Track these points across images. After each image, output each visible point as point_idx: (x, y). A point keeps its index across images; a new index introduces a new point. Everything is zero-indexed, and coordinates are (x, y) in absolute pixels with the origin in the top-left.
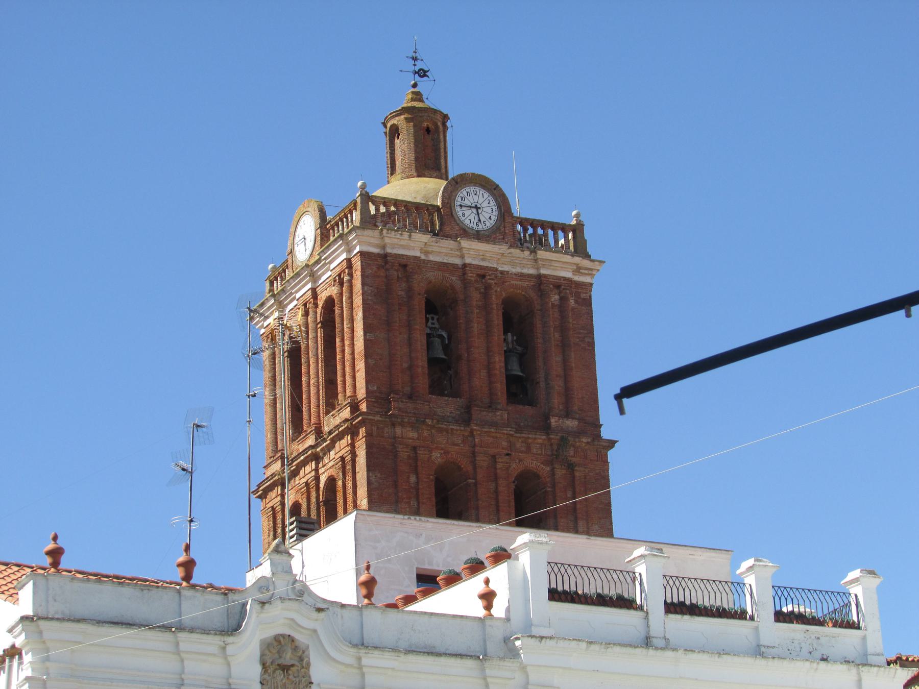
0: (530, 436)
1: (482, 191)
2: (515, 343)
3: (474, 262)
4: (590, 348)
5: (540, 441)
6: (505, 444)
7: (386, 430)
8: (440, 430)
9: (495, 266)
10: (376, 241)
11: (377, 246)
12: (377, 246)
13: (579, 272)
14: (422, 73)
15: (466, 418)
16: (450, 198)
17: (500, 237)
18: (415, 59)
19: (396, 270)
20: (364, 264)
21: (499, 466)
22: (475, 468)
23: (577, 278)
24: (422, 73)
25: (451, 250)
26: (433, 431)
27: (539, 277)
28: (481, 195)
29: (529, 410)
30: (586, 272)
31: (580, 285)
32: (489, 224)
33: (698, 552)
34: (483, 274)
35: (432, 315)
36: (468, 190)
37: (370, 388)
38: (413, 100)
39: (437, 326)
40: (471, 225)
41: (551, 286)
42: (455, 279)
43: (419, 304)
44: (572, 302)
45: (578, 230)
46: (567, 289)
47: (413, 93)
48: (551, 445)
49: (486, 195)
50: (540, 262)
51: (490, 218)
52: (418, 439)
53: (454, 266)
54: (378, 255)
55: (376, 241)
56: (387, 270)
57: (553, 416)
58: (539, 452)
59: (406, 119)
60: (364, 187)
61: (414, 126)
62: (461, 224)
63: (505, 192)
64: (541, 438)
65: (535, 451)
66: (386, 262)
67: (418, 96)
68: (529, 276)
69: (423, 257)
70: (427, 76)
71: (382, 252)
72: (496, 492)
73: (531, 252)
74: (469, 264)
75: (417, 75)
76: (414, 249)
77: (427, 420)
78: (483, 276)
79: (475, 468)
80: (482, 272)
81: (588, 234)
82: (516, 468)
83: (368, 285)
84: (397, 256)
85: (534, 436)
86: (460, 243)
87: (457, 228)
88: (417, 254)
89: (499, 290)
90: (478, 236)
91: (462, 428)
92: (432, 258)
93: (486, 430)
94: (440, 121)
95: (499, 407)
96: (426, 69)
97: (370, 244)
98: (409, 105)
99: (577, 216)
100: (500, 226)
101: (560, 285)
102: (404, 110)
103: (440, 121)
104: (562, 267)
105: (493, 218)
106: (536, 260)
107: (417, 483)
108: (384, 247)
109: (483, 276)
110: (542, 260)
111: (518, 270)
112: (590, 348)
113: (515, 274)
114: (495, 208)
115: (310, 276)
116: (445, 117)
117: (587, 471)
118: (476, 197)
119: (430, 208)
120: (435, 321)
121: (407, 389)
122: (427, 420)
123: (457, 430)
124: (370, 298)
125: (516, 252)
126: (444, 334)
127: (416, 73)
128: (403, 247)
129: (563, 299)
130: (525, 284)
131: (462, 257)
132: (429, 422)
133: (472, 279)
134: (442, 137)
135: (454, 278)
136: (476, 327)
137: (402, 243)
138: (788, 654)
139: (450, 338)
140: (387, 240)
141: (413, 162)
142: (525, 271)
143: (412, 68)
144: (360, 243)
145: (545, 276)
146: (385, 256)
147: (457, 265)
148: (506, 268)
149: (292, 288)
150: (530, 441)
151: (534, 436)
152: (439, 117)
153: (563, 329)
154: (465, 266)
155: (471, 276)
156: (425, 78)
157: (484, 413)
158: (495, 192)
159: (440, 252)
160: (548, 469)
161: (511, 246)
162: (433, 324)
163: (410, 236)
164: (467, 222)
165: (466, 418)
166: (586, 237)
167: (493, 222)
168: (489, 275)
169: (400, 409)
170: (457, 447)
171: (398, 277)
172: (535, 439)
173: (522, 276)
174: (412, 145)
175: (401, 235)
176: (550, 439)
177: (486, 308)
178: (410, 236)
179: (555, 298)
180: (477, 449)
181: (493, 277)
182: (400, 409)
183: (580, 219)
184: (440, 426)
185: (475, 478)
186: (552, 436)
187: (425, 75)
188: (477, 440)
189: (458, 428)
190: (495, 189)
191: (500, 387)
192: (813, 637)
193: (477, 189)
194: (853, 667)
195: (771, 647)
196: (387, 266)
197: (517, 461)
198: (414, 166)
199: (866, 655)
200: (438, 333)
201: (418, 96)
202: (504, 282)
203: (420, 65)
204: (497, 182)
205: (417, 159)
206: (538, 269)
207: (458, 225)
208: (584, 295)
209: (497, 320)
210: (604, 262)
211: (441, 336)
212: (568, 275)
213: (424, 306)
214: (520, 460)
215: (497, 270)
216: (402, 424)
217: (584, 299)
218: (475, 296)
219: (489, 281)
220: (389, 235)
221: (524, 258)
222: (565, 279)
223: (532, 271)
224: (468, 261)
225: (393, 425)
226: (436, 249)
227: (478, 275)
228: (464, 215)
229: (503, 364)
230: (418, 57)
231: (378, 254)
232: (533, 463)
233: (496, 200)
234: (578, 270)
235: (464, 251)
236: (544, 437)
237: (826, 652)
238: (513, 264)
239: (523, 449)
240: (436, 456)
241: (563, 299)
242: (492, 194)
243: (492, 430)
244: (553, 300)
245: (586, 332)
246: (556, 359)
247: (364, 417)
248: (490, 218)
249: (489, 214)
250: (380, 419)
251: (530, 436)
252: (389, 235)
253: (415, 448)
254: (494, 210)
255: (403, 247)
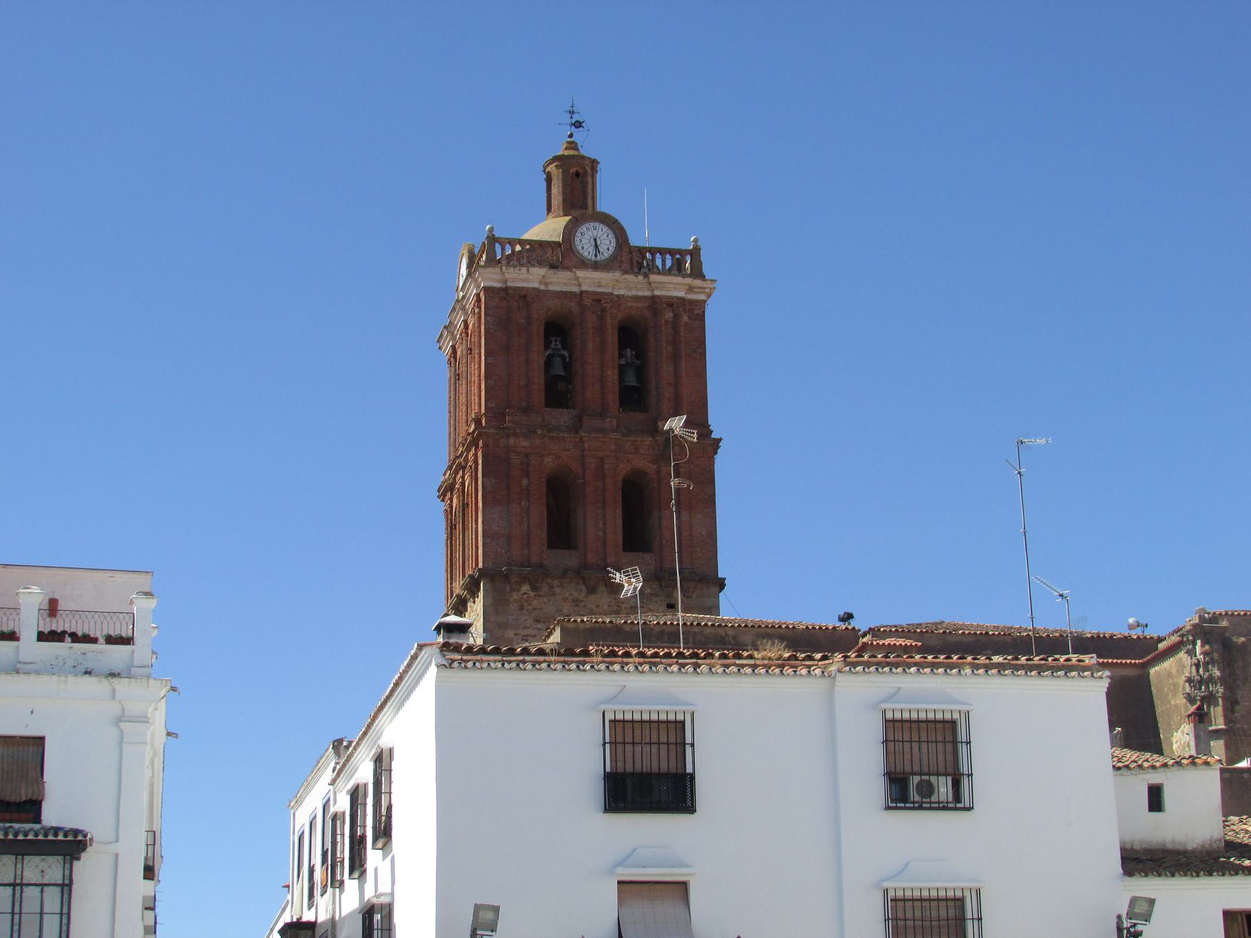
0: (638, 439)
1: (602, 226)
2: (633, 357)
3: (590, 289)
4: (702, 358)
5: (647, 443)
6: (613, 447)
7: (502, 440)
8: (552, 438)
9: (610, 291)
10: (498, 277)
11: (499, 281)
12: (499, 281)
13: (692, 291)
14: (578, 125)
15: (576, 427)
16: (570, 234)
17: (618, 265)
18: (572, 112)
19: (516, 301)
20: (487, 297)
21: (606, 466)
22: (584, 470)
23: (690, 297)
24: (578, 125)
25: (569, 279)
26: (546, 439)
27: (653, 298)
28: (600, 230)
29: (640, 416)
30: (699, 290)
31: (692, 302)
32: (607, 255)
33: (118, 575)
34: (598, 299)
35: (554, 338)
36: (588, 226)
37: (489, 405)
38: (567, 149)
39: (559, 347)
40: (590, 256)
41: (664, 305)
42: (573, 306)
43: (538, 330)
44: (685, 318)
45: (695, 253)
46: (679, 307)
47: (568, 142)
48: (658, 445)
49: (605, 229)
50: (653, 285)
51: (608, 249)
52: (530, 447)
53: (573, 294)
54: (501, 289)
55: (498, 277)
56: (508, 301)
57: (660, 420)
58: (647, 452)
59: (556, 166)
60: (491, 230)
61: (563, 172)
62: (579, 256)
63: (624, 226)
64: (648, 440)
65: (643, 451)
66: (507, 294)
67: (572, 145)
68: (645, 297)
69: (542, 287)
70: (583, 127)
71: (504, 286)
72: (604, 489)
73: (645, 277)
74: (585, 291)
75: (573, 127)
76: (533, 282)
77: (538, 430)
78: (599, 301)
79: (584, 470)
80: (595, 297)
81: (704, 257)
82: (624, 469)
83: (489, 315)
84: (516, 289)
85: (641, 439)
86: (575, 274)
87: (576, 259)
88: (536, 285)
89: (615, 311)
90: (596, 266)
91: (572, 435)
92: (551, 288)
93: (593, 436)
94: (588, 166)
95: (609, 415)
96: (582, 121)
97: (492, 280)
98: (566, 153)
99: (696, 241)
100: (618, 254)
101: (672, 303)
102: (556, 159)
103: (588, 166)
104: (675, 288)
105: (610, 249)
106: (650, 283)
107: (528, 486)
108: (505, 282)
109: (599, 301)
110: (655, 282)
111: (634, 293)
112: (702, 358)
113: (631, 297)
114: (613, 240)
115: (462, 309)
116: (594, 163)
117: (692, 466)
118: (595, 232)
119: (552, 244)
120: (558, 342)
121: (524, 404)
122: (538, 430)
123: (567, 437)
124: (491, 327)
125: (631, 277)
126: (566, 354)
127: (572, 124)
128: (523, 280)
129: (676, 316)
130: (641, 305)
131: (580, 285)
132: (539, 432)
133: (589, 304)
134: (589, 179)
135: (572, 304)
136: (590, 346)
137: (522, 277)
138: (52, 669)
139: (570, 357)
140: (507, 276)
141: (561, 203)
142: (641, 293)
143: (569, 121)
144: (484, 279)
145: (659, 297)
146: (506, 290)
147: (575, 292)
148: (622, 292)
149: (455, 318)
150: (638, 443)
151: (641, 439)
152: (587, 162)
153: (675, 342)
154: (582, 292)
155: (588, 302)
156: (581, 128)
157: (594, 421)
158: (614, 226)
159: (559, 283)
160: (655, 467)
161: (626, 272)
162: (556, 345)
163: (528, 270)
164: (586, 254)
165: (576, 427)
166: (702, 259)
167: (610, 252)
168: (605, 300)
169: (514, 422)
170: (568, 452)
171: (519, 306)
172: (642, 441)
173: (637, 298)
174: (561, 189)
175: (520, 270)
176: (656, 441)
177: (601, 329)
178: (528, 270)
179: (669, 315)
180: (586, 453)
181: (608, 301)
182: (514, 422)
183: (698, 244)
184: (552, 434)
185: (584, 479)
186: (657, 438)
187: (580, 126)
188: (586, 445)
189: (568, 435)
190: (613, 223)
191: (613, 396)
192: (79, 653)
193: (597, 224)
194: (104, 679)
195: (27, 663)
196: (508, 298)
197: (626, 462)
198: (561, 207)
199: (131, 665)
200: (560, 353)
201: (572, 145)
202: (620, 305)
203: (576, 118)
204: (616, 217)
205: (564, 200)
206: (653, 291)
207: (577, 257)
208: (698, 311)
209: (612, 339)
210: (716, 281)
211: (563, 357)
212: (681, 294)
213: (543, 331)
214: (628, 461)
215: (612, 294)
216: (515, 435)
217: (698, 315)
218: (591, 319)
219: (605, 305)
220: (508, 271)
221: (638, 282)
222: (678, 298)
223: (647, 293)
224: (584, 288)
225: (508, 436)
226: (554, 280)
227: (594, 300)
228: (583, 248)
229: (616, 377)
230: (575, 111)
231: (501, 288)
232: (640, 463)
233: (615, 234)
234: (691, 289)
235: (581, 280)
236: (650, 439)
237: (90, 666)
238: (630, 289)
239: (632, 451)
240: (548, 461)
241: (676, 316)
242: (611, 228)
243: (600, 436)
244: (667, 317)
245: (698, 344)
246: (667, 370)
247: (480, 430)
248: (608, 249)
249: (608, 244)
250: (496, 431)
251: (638, 439)
252: (508, 271)
253: (527, 455)
254: (578, 241)
255: (523, 280)
